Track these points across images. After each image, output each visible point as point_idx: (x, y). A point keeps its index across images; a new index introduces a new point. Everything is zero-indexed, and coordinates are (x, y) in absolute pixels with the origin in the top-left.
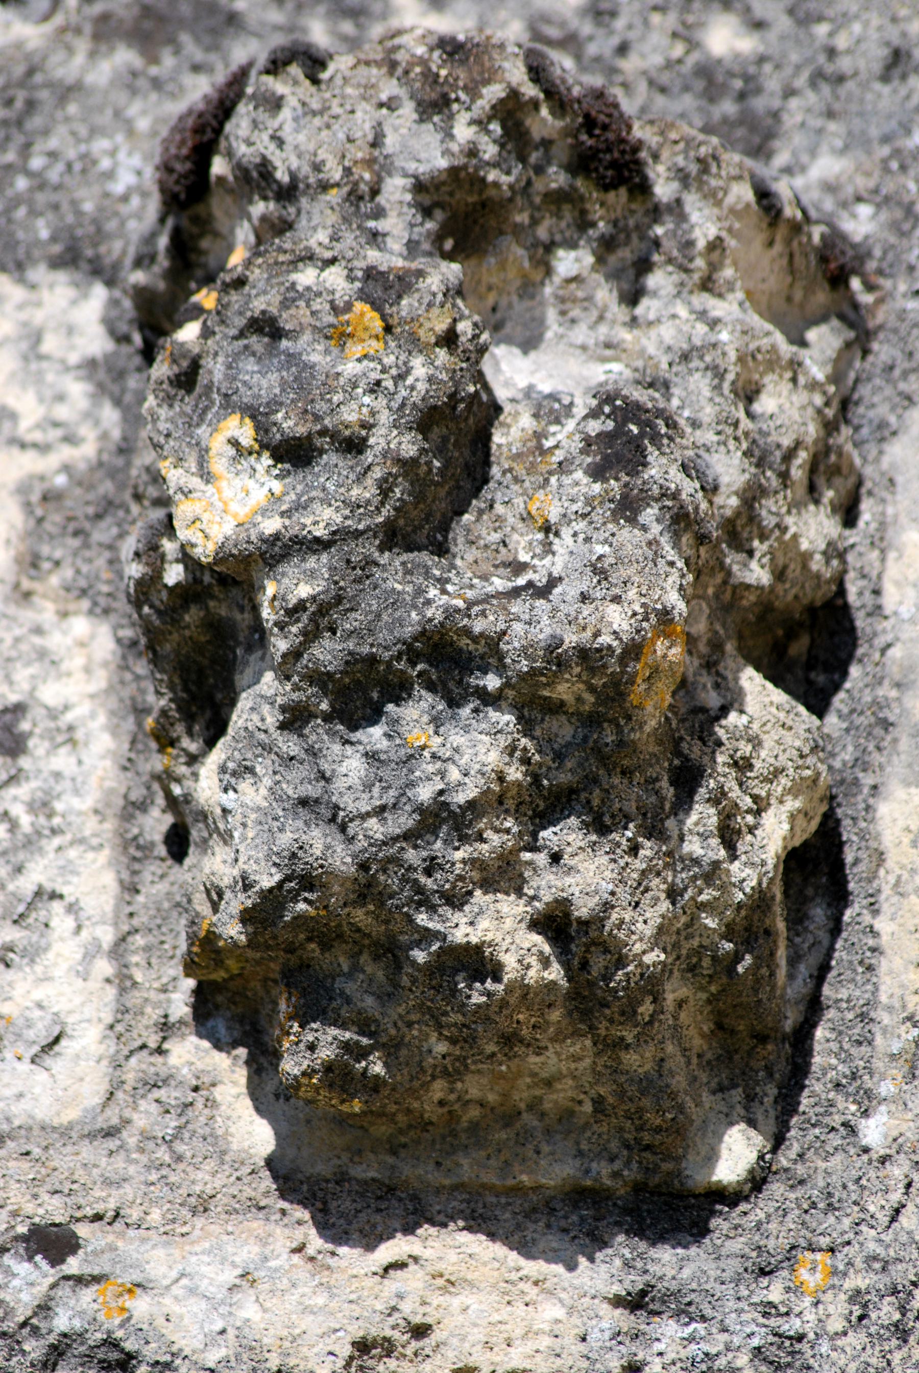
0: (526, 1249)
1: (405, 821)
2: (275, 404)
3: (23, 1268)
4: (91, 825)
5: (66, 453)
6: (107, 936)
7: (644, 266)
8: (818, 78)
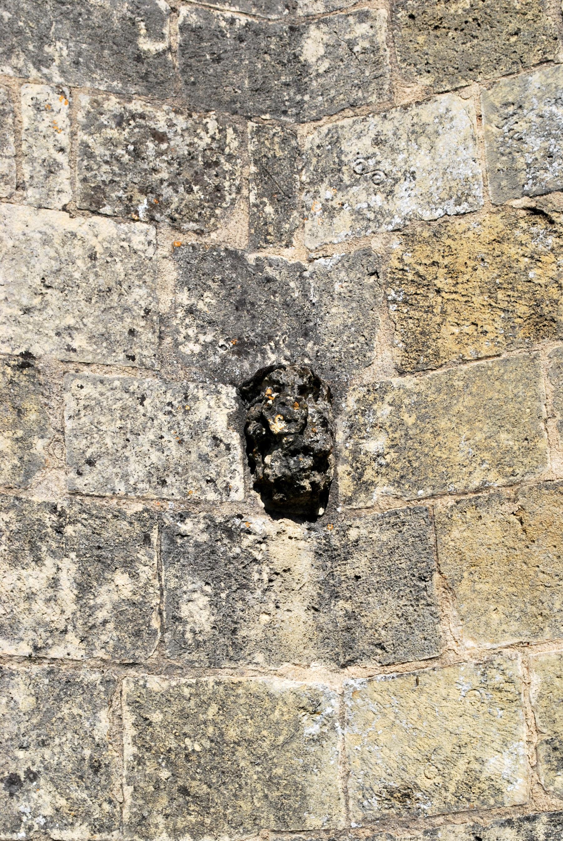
0: (297, 522)
1: (297, 470)
2: (286, 415)
3: (237, 520)
4: (239, 461)
5: (232, 410)
6: (243, 476)
7: (318, 397)
8: (319, 368)
